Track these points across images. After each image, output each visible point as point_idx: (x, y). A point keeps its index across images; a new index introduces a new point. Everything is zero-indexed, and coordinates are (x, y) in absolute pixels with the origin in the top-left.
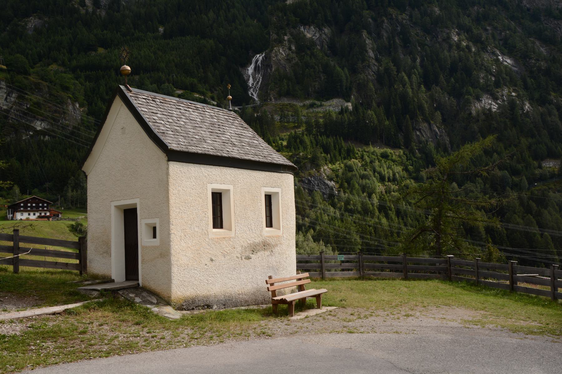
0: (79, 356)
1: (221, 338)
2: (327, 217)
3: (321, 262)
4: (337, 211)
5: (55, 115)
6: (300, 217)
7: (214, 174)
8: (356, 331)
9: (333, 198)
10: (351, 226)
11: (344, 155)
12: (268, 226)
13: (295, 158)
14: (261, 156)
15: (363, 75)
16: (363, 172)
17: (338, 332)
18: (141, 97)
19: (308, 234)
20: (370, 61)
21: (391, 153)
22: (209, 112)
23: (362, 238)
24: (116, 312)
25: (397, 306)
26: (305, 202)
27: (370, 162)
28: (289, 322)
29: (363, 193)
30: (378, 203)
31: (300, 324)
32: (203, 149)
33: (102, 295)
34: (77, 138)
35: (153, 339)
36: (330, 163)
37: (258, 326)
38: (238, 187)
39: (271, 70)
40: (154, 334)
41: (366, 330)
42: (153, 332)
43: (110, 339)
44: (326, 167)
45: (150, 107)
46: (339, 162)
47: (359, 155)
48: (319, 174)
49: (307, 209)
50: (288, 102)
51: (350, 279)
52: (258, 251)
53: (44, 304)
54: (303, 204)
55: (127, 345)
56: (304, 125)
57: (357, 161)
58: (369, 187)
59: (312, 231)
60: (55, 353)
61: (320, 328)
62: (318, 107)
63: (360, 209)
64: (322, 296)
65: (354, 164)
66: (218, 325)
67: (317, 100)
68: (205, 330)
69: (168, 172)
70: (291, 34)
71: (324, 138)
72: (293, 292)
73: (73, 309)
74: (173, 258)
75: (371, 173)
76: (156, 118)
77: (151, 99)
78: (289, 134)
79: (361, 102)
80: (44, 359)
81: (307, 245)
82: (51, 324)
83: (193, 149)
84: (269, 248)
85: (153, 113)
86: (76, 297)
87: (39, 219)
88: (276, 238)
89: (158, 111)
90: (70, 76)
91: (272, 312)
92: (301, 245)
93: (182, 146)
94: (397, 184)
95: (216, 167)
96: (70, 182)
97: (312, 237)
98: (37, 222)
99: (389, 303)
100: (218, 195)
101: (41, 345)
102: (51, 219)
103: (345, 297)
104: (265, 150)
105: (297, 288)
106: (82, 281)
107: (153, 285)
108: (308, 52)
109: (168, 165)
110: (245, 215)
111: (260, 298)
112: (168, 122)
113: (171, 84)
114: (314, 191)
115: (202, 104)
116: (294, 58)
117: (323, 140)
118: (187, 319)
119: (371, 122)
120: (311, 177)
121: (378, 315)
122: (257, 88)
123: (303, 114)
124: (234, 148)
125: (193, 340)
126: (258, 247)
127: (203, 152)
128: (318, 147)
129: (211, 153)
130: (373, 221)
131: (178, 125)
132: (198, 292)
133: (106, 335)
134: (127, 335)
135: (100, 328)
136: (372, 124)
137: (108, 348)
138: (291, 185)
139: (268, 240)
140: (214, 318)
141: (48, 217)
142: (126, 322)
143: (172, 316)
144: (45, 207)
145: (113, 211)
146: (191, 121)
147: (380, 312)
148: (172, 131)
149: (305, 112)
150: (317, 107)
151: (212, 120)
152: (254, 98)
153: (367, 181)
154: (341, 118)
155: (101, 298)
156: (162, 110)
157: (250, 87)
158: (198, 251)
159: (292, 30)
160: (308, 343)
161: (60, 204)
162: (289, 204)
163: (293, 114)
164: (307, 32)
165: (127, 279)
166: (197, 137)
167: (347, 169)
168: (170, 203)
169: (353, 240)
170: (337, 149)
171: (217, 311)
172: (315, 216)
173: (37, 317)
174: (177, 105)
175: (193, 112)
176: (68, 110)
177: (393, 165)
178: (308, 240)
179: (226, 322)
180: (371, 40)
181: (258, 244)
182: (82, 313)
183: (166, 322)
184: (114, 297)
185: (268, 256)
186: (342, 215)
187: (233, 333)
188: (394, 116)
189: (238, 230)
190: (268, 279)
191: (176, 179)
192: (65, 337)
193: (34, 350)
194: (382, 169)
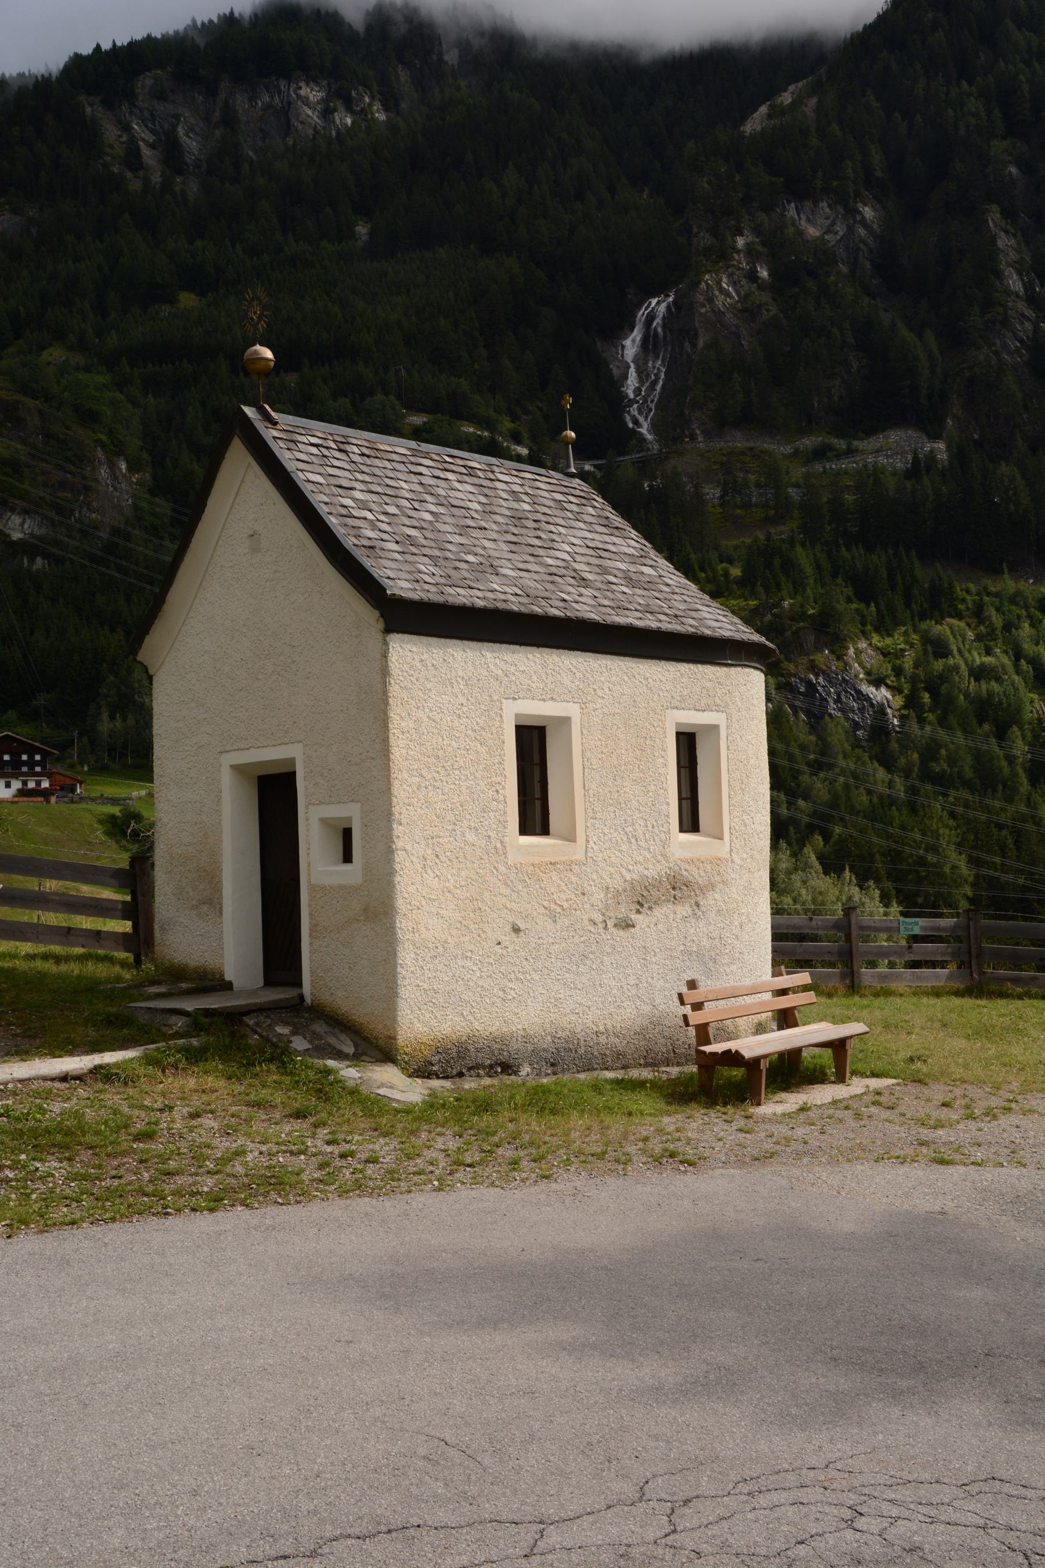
0: (136, 1204)
1: (544, 1167)
2: (864, 798)
3: (848, 938)
4: (897, 779)
5: (60, 494)
6: (783, 797)
7: (523, 672)
8: (958, 1157)
9: (883, 737)
10: (940, 825)
12: (685, 827)
13: (769, 618)
14: (666, 614)
16: (979, 659)
17: (902, 1161)
18: (303, 439)
19: (805, 850)
20: (1010, 304)
22: (506, 483)
23: (973, 861)
24: (238, 1079)
26: (797, 751)
27: (1003, 628)
28: (750, 1123)
29: (980, 724)
30: (1029, 756)
31: (782, 1130)
32: (490, 595)
33: (196, 1027)
34: (124, 563)
35: (343, 1163)
36: (877, 629)
37: (655, 1131)
38: (595, 710)
39: (694, 345)
40: (347, 1146)
41: (992, 1156)
42: (345, 1140)
43: (222, 1158)
44: (863, 645)
45: (331, 471)
46: (904, 629)
47: (970, 606)
48: (841, 664)
49: (803, 773)
51: (937, 993)
52: (655, 903)
53: (38, 1048)
54: (791, 758)
55: (270, 1177)
57: (962, 624)
59: (818, 839)
60: (68, 1192)
61: (847, 1144)
62: (839, 455)
63: (969, 773)
64: (850, 1046)
65: (952, 633)
66: (534, 1126)
67: (837, 437)
68: (496, 1139)
69: (387, 666)
70: (757, 231)
72: (760, 1029)
73: (117, 1065)
74: (401, 923)
75: (1006, 660)
76: (348, 502)
77: (333, 446)
78: (748, 541)
79: (976, 436)
80: (40, 1209)
81: (804, 882)
82: (56, 1107)
83: (460, 596)
84: (689, 896)
85: (340, 487)
86: (125, 1030)
87: (21, 799)
88: (709, 867)
89: (356, 480)
90: (101, 379)
91: (696, 1088)
92: (784, 881)
93: (427, 587)
95: (529, 648)
96: (105, 691)
97: (818, 858)
98: (15, 806)
100: (535, 733)
101: (32, 1168)
102: (53, 799)
103: (924, 1048)
104: (676, 597)
105: (773, 1018)
106: (140, 985)
107: (342, 1001)
108: (811, 284)
109: (386, 643)
111: (662, 1047)
112: (386, 513)
113: (392, 397)
114: (826, 717)
115: (485, 457)
116: (766, 304)
118: (443, 1106)
120: (817, 675)
121: (1030, 1110)
122: (652, 401)
123: (794, 480)
124: (582, 590)
125: (462, 1168)
126: (654, 892)
127: (490, 605)
128: (840, 580)
129: (515, 608)
130: (1011, 809)
131: (416, 524)
132: (476, 1025)
133: (208, 1146)
134: (270, 1149)
135: (194, 1123)
137: (215, 1185)
138: (756, 702)
139: (686, 870)
140: (523, 1105)
141: (45, 794)
142: (265, 1108)
143: (397, 1095)
144: (38, 763)
145: (227, 780)
146: (452, 509)
148: (397, 542)
149: (798, 472)
150: (836, 456)
151: (515, 505)
152: (640, 433)
153: (995, 686)
155: (194, 1037)
156: (367, 478)
157: (630, 400)
158: (475, 903)
159: (762, 217)
160: (810, 1189)
161: (78, 757)
162: (752, 762)
163: (763, 479)
164: (808, 220)
165: (270, 980)
166: (471, 558)
167: (929, 648)
168: (392, 757)
169: (947, 869)
171: (532, 1082)
172: (830, 793)
173: (19, 1085)
174: (412, 463)
175: (459, 481)
176: (97, 480)
178: (806, 867)
179: (558, 1118)
180: (1014, 235)
181: (656, 885)
182: (142, 1080)
183: (382, 1112)
184: (232, 1035)
185: (685, 918)
186: (913, 791)
187: (581, 1152)
189: (595, 838)
190: (684, 990)
191: (409, 685)
192: (96, 1147)
193: (11, 1180)
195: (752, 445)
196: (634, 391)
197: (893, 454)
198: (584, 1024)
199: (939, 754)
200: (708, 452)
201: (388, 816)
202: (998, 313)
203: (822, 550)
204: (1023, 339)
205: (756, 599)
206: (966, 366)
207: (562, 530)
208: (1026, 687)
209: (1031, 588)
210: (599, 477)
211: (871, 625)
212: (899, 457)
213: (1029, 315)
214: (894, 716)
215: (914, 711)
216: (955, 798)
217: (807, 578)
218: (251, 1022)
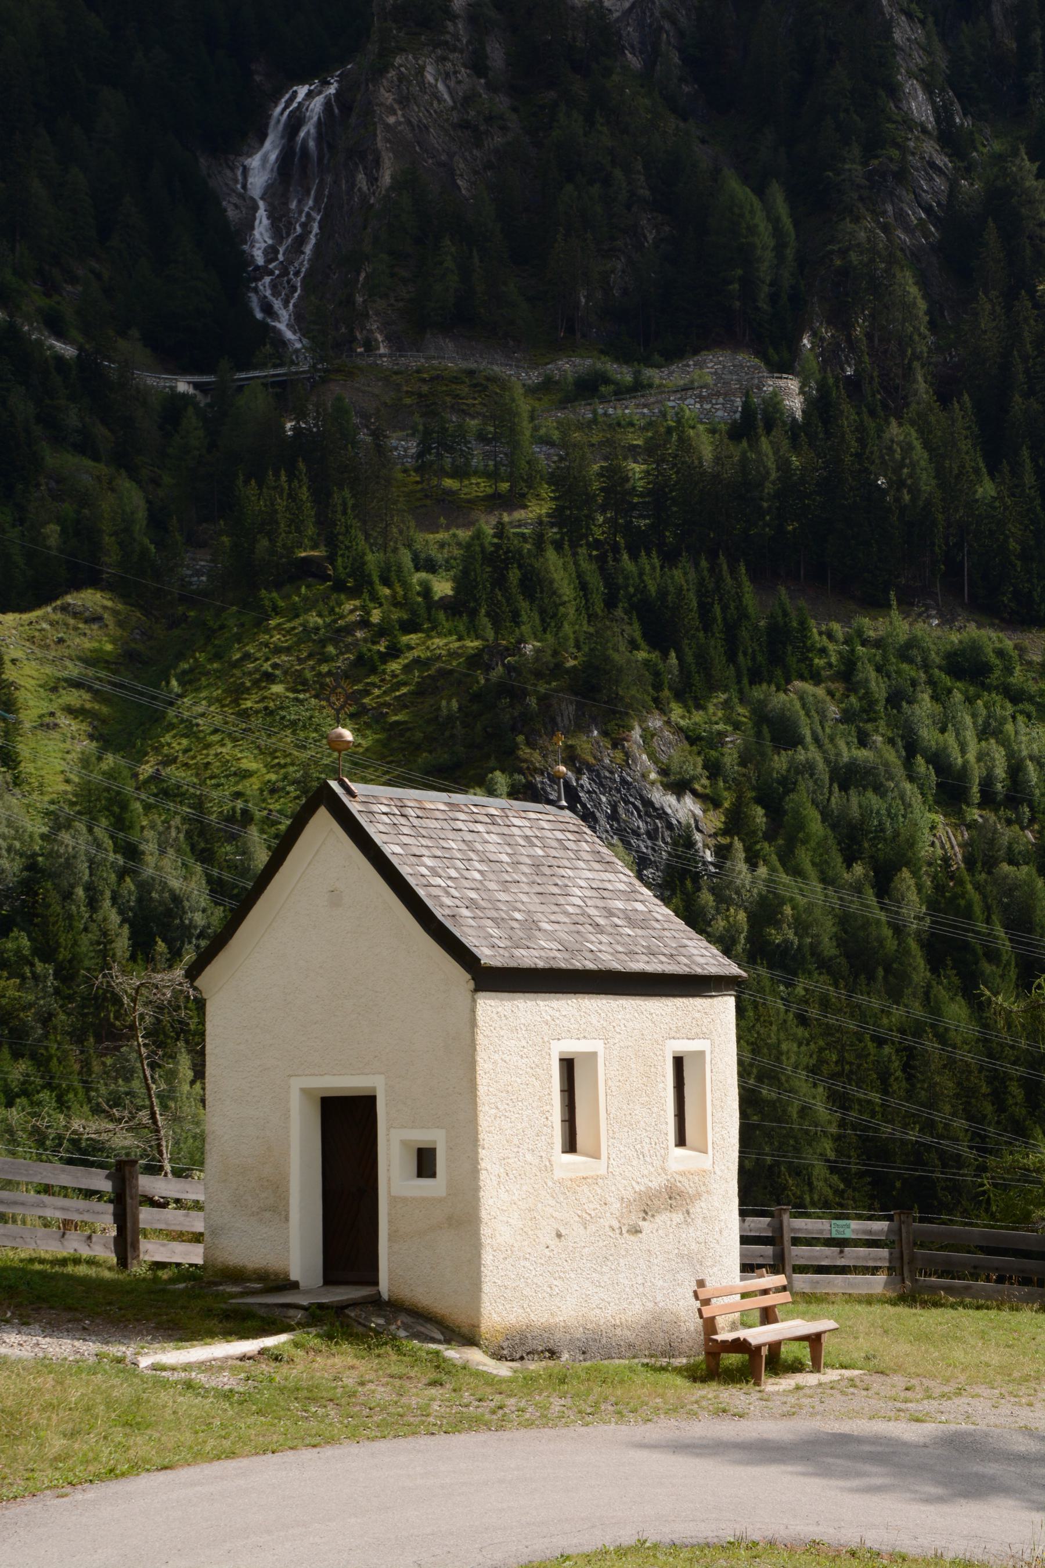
9: (689, 884)
10: (782, 1035)
11: (754, 659)
15: (868, 223)
16: (848, 752)
20: (912, 144)
21: (1000, 653)
23: (839, 1100)
25: (1026, 1378)
27: (888, 700)
39: (373, 180)
44: (656, 722)
46: (723, 697)
47: (834, 660)
48: (619, 755)
50: (464, 365)
56: (546, 491)
57: (820, 691)
58: (883, 830)
62: (622, 392)
63: (829, 948)
64: (825, 1338)
65: (804, 706)
67: (616, 360)
71: (650, 562)
73: (276, 1347)
75: (892, 757)
78: (464, 534)
84: (682, 1205)
94: (1032, 820)
99: (1005, 1371)
104: (666, 933)
107: (423, 1296)
109: (474, 1001)
110: (629, 1118)
117: (641, 574)
119: (901, 484)
120: (579, 772)
122: (297, 273)
128: (619, 613)
130: (898, 1012)
136: (907, 498)
147: (982, 1390)
150: (616, 393)
153: (873, 800)
154: (744, 460)
157: (257, 268)
167: (765, 730)
170: (719, 625)
177: (1014, 717)
180: (922, 22)
188: (1025, 453)
189: (614, 1156)
191: (489, 1034)
194: (950, 738)
195: (473, 366)
196: (266, 252)
197: (710, 395)
198: (606, 1317)
199: (782, 914)
200: (396, 373)
201: (474, 1142)
202: (891, 160)
203: (590, 555)
204: (931, 206)
205: (477, 638)
206: (836, 248)
207: (570, 873)
208: (924, 802)
209: (934, 634)
210: (202, 405)
211: (670, 689)
212: (721, 400)
213: (941, 165)
214: (706, 846)
215: (740, 839)
216: (806, 990)
217: (564, 604)
218: (352, 1314)
